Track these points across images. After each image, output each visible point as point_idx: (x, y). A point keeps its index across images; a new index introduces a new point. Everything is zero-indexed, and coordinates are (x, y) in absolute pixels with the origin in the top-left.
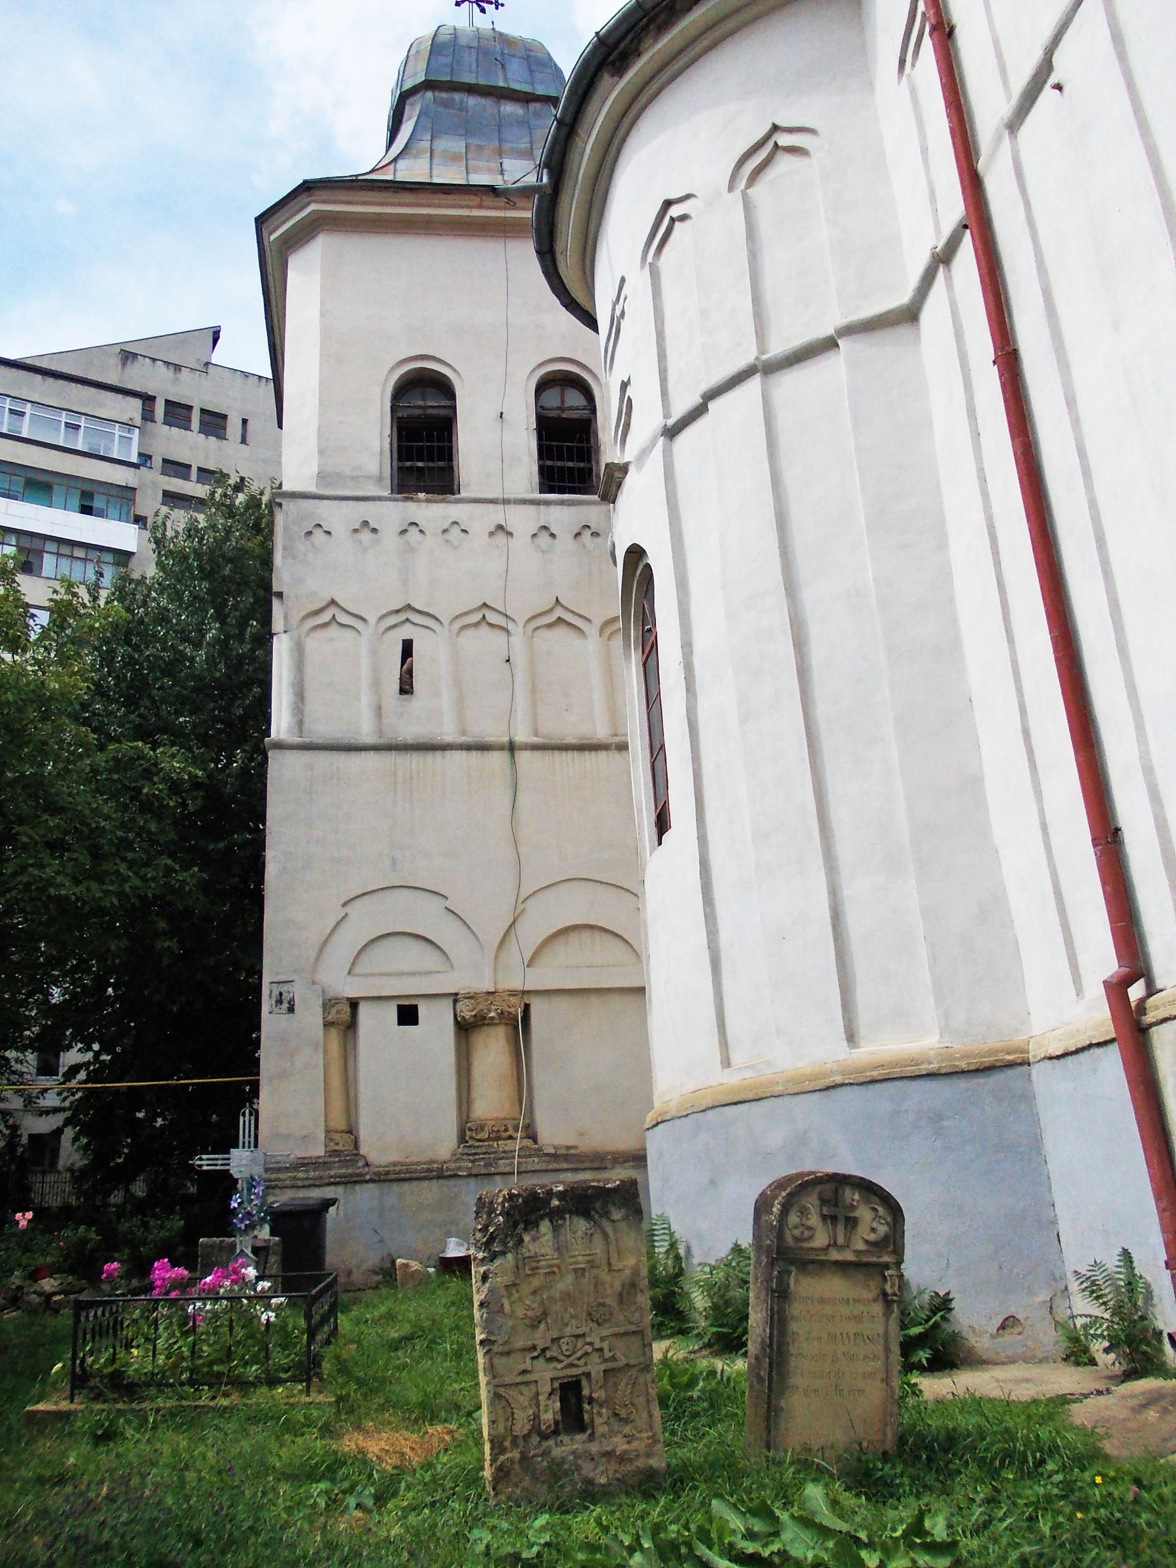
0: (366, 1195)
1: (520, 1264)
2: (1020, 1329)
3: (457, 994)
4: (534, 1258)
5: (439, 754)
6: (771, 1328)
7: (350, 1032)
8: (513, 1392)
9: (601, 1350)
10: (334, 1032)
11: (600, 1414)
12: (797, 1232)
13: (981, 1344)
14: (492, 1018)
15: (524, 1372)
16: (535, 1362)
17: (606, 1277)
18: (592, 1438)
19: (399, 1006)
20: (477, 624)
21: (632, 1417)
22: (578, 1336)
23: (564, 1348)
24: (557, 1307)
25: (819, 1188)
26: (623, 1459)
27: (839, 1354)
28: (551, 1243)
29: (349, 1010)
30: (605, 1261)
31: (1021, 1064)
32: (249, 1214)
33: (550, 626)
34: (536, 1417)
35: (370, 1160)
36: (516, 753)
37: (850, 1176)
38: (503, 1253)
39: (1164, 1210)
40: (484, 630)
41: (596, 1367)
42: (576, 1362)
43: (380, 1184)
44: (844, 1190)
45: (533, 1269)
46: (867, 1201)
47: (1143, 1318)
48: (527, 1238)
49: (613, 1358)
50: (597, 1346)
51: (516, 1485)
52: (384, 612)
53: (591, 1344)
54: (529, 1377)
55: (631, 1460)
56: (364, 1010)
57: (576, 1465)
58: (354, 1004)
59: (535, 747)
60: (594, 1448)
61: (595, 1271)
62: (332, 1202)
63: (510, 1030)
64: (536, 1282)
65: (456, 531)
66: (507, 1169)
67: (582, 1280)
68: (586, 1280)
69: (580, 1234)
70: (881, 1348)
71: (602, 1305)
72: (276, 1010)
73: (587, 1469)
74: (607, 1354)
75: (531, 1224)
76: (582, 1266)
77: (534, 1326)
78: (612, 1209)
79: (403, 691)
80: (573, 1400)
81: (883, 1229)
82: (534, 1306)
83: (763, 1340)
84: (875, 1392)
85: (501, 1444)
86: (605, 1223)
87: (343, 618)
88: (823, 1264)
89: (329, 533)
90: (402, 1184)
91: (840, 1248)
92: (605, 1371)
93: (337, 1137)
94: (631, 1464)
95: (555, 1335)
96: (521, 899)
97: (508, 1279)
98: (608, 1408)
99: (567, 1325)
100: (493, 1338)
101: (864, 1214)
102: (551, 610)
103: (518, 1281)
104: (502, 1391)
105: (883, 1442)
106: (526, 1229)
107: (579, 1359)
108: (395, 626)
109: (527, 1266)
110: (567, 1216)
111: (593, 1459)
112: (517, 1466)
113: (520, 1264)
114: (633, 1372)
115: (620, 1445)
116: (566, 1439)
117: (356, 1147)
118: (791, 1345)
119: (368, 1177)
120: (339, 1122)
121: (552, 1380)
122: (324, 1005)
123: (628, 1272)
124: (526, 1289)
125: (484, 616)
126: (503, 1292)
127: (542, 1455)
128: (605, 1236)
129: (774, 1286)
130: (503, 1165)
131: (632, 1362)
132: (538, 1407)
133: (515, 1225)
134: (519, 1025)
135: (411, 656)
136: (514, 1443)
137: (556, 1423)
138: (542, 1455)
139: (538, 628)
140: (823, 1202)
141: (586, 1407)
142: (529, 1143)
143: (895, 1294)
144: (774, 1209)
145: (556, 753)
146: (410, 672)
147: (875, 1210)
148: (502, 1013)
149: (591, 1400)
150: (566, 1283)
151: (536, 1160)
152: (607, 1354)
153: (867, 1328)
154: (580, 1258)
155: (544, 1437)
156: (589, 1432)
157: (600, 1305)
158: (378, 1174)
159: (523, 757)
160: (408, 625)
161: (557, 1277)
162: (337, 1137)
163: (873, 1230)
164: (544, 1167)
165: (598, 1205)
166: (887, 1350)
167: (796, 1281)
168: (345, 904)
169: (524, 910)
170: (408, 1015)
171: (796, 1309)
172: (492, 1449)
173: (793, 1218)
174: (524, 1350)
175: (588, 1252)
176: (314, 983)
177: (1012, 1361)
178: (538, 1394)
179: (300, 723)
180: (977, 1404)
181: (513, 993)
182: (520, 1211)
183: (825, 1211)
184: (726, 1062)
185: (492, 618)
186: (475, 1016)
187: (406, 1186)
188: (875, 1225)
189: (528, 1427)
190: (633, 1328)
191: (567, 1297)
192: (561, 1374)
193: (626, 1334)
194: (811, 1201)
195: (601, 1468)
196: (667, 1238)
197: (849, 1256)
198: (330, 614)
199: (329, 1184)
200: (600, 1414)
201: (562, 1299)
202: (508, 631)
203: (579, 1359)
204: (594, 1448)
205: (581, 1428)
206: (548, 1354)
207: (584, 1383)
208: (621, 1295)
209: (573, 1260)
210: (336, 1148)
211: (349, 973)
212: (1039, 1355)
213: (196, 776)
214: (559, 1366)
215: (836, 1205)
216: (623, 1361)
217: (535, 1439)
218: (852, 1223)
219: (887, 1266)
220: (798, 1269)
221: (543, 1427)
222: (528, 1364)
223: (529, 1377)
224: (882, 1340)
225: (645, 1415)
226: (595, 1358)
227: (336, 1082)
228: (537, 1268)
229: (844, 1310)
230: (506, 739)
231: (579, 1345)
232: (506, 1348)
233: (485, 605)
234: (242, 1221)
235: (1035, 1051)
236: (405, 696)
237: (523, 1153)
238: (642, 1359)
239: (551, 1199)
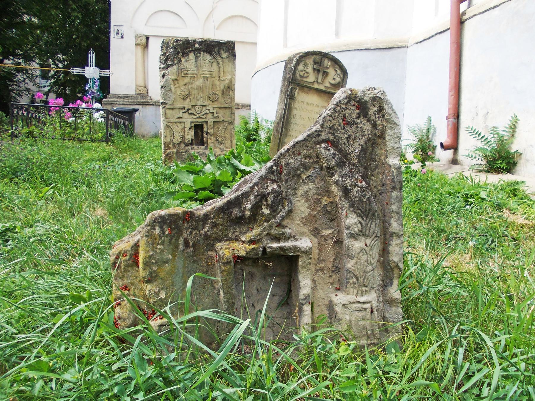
1: (180, 71)
8: (174, 125)
9: (213, 113)
10: (139, 47)
11: (210, 139)
12: (302, 74)
15: (179, 118)
16: (184, 114)
17: (217, 83)
18: (206, 148)
22: (203, 106)
23: (197, 110)
24: (195, 92)
25: (315, 56)
28: (194, 64)
29: (145, 40)
30: (217, 75)
31: (404, 47)
32: (93, 92)
34: (184, 137)
38: (172, 65)
39: (452, 96)
41: (210, 119)
45: (185, 74)
46: (334, 67)
47: (430, 141)
48: (183, 60)
49: (218, 117)
50: (211, 111)
53: (209, 110)
54: (181, 120)
56: (151, 40)
58: (147, 38)
61: (213, 79)
62: (137, 110)
64: (187, 80)
69: (207, 61)
72: (116, 37)
74: (215, 115)
75: (185, 55)
78: (222, 52)
80: (200, 133)
81: (338, 80)
82: (184, 90)
83: (281, 116)
85: (168, 146)
88: (310, 89)
93: (140, 88)
97: (174, 77)
98: (214, 137)
99: (199, 100)
104: (169, 124)
106: (183, 56)
107: (203, 115)
109: (182, 73)
110: (202, 52)
112: (174, 155)
113: (180, 71)
114: (226, 124)
116: (196, 147)
117: (147, 93)
118: (292, 119)
121: (191, 122)
122: (136, 37)
123: (227, 82)
124: (181, 83)
126: (171, 82)
128: (218, 63)
129: (288, 93)
131: (226, 120)
132: (185, 133)
133: (178, 53)
140: (315, 63)
141: (205, 135)
144: (293, 62)
149: (207, 133)
150: (199, 82)
152: (215, 115)
154: (207, 72)
155: (187, 145)
157: (214, 93)
158: (155, 102)
161: (196, 79)
162: (140, 88)
163: (334, 79)
165: (216, 50)
167: (298, 94)
171: (296, 105)
172: (165, 147)
173: (301, 67)
174: (180, 108)
176: (131, 27)
178: (185, 127)
182: (180, 48)
183: (315, 66)
184: (285, 46)
188: (335, 77)
189: (180, 140)
190: (227, 106)
191: (200, 88)
192: (194, 120)
193: (225, 108)
194: (310, 62)
197: (322, 87)
200: (210, 139)
201: (197, 89)
203: (203, 115)
205: (203, 144)
206: (190, 111)
207: (205, 126)
208: (223, 91)
209: (203, 72)
215: (320, 66)
216: (221, 119)
217: (183, 145)
218: (325, 74)
220: (300, 89)
221: (186, 141)
222: (181, 115)
223: (181, 120)
225: (229, 142)
226: (210, 116)
227: (140, 68)
228: (187, 74)
231: (204, 110)
232: (172, 107)
234: (90, 95)
235: (411, 41)
238: (230, 119)
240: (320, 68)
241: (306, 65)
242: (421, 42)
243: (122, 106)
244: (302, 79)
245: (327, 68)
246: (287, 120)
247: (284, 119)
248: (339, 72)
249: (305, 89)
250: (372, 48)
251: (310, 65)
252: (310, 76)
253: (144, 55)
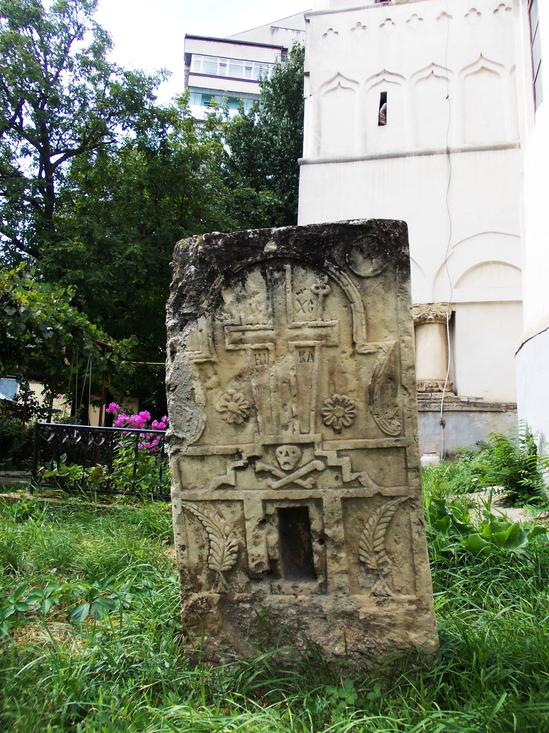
4: (239, 327)
5: (401, 159)
8: (210, 512)
9: (338, 468)
11: (335, 558)
14: (431, 319)
15: (224, 486)
16: (240, 474)
17: (349, 364)
18: (323, 589)
20: (428, 77)
21: (386, 570)
22: (303, 446)
23: (282, 459)
24: (271, 399)
26: (369, 625)
28: (263, 307)
30: (345, 338)
33: (476, 73)
34: (241, 550)
36: (451, 155)
38: (194, 317)
41: (330, 492)
42: (300, 481)
45: (235, 342)
48: (228, 298)
50: (333, 461)
51: (213, 634)
52: (369, 77)
53: (323, 458)
54: (229, 494)
55: (382, 630)
57: (299, 622)
59: (464, 151)
60: (327, 603)
61: (332, 352)
63: (442, 328)
64: (242, 362)
65: (415, 19)
66: (436, 409)
67: (310, 364)
68: (316, 364)
71: (343, 403)
73: (316, 631)
75: (235, 278)
76: (311, 343)
77: (237, 426)
79: (380, 124)
85: (194, 579)
86: (346, 280)
87: (344, 84)
89: (336, 33)
92: (344, 500)
94: (382, 635)
95: (269, 440)
99: (286, 427)
100: (181, 435)
102: (477, 62)
103: (214, 358)
104: (193, 507)
106: (227, 284)
107: (304, 477)
108: (376, 85)
110: (288, 267)
111: (325, 618)
113: (218, 333)
114: (391, 506)
115: (368, 607)
116: (287, 585)
121: (265, 502)
123: (382, 357)
124: (226, 371)
125: (433, 71)
126: (193, 371)
127: (251, 601)
130: (433, 407)
131: (388, 491)
132: (245, 536)
134: (449, 324)
136: (212, 575)
137: (272, 562)
138: (251, 601)
139: (468, 75)
141: (316, 546)
142: (451, 394)
145: (478, 153)
146: (385, 112)
148: (437, 316)
149: (323, 539)
150: (284, 366)
151: (455, 404)
152: (348, 476)
154: (308, 331)
156: (320, 580)
157: (337, 402)
160: (384, 83)
161: (272, 357)
164: (459, 408)
165: (336, 253)
169: (453, 253)
174: (224, 456)
175: (319, 322)
178: (243, 520)
179: (319, 148)
181: (444, 304)
182: (219, 258)
185: (437, 72)
186: (420, 318)
189: (230, 561)
190: (387, 442)
191: (288, 388)
192: (276, 495)
193: (380, 450)
195: (338, 632)
196: (525, 428)
198: (338, 81)
200: (335, 558)
201: (277, 389)
202: (447, 79)
203: (304, 477)
204: (327, 603)
207: (313, 512)
208: (370, 392)
213: (279, 204)
214: (276, 484)
217: (241, 579)
221: (252, 565)
222: (229, 477)
223: (229, 494)
225: (406, 569)
226: (329, 478)
228: (241, 341)
230: (444, 148)
232: (198, 450)
233: (433, 64)
236: (381, 127)
237: (447, 400)
239: (266, 241)
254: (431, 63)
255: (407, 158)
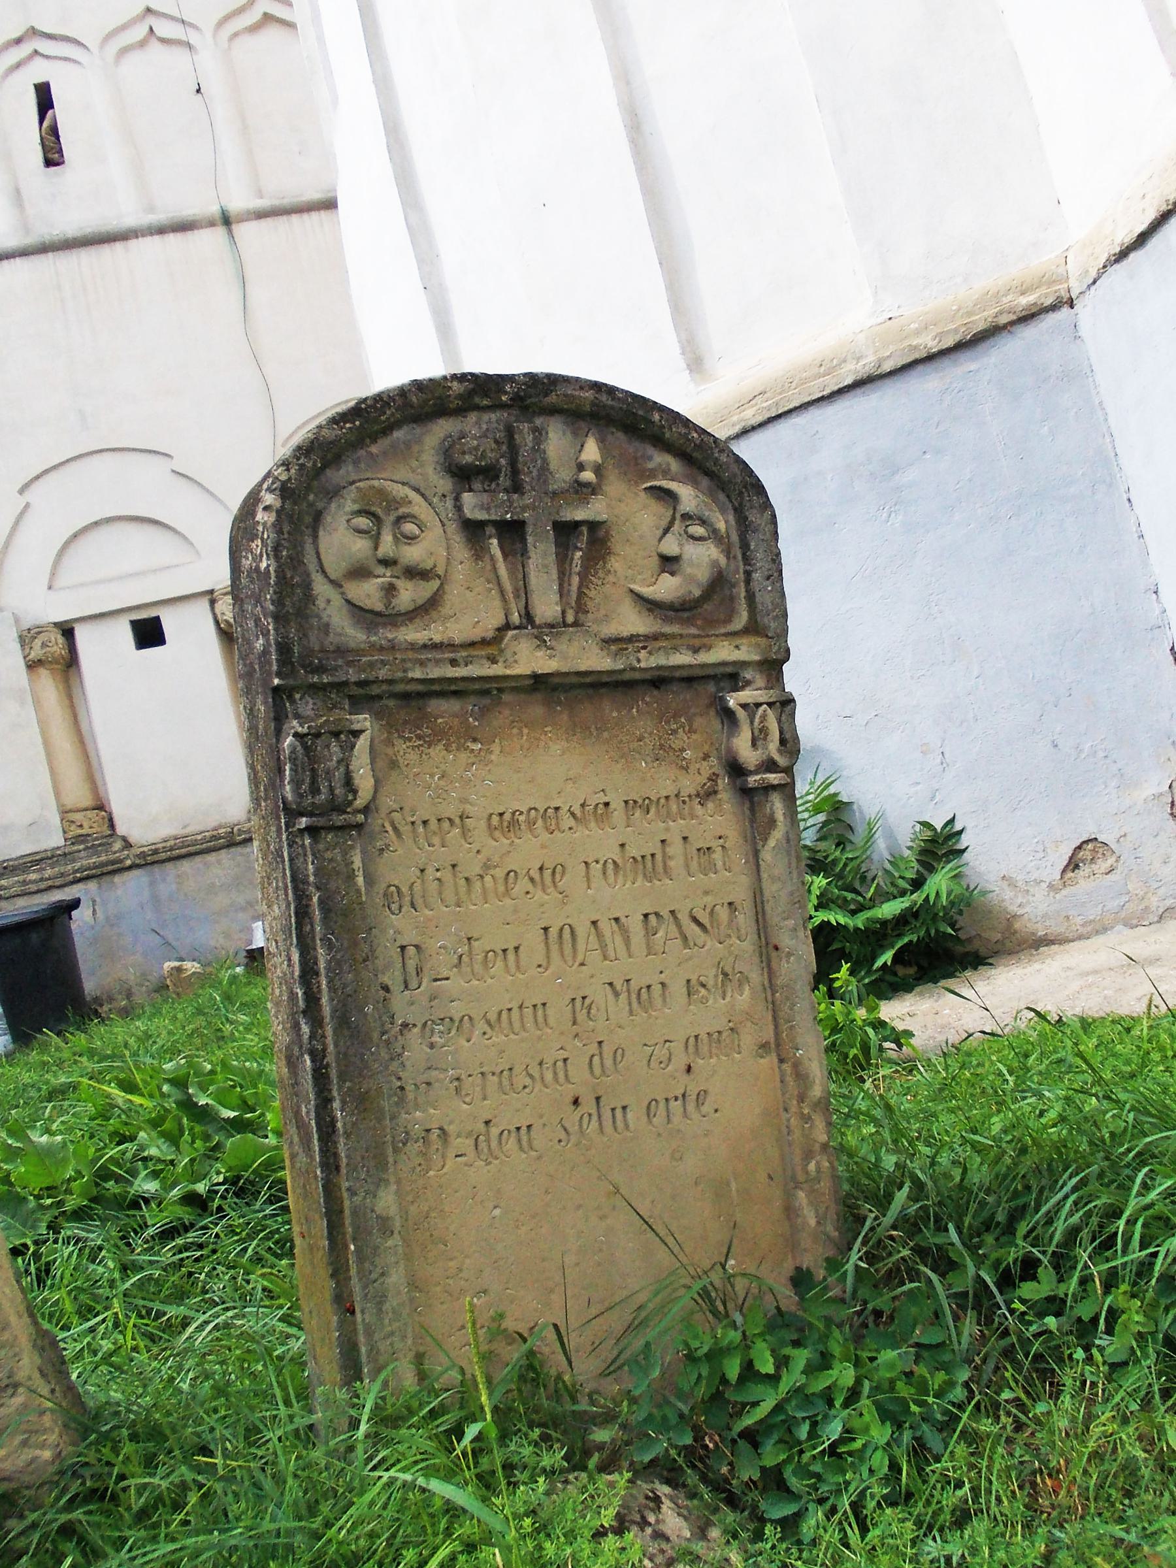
0: (130, 889)
2: (1111, 861)
3: (212, 592)
5: (119, 246)
6: (306, 948)
7: (73, 669)
10: (43, 672)
12: (368, 592)
13: (1034, 908)
19: (133, 623)
20: (142, 44)
25: (443, 427)
27: (599, 994)
29: (61, 640)
31: (1054, 308)
33: (254, 28)
35: (131, 840)
36: (234, 227)
37: (553, 381)
40: (155, 47)
43: (149, 868)
44: (539, 434)
46: (637, 471)
56: (82, 635)
58: (67, 631)
59: (261, 215)
62: (75, 904)
70: (747, 946)
79: (49, 163)
81: (702, 557)
84: (739, 1091)
88: (488, 691)
90: (178, 863)
91: (544, 633)
93: (78, 817)
96: (279, 441)
101: (627, 510)
105: (792, 1244)
108: (18, 66)
117: (112, 825)
119: (128, 862)
120: (78, 795)
122: (22, 639)
135: (52, 107)
143: (770, 766)
145: (295, 218)
146: (54, 131)
147: (667, 496)
153: (681, 891)
158: (143, 855)
159: (244, 231)
160: (38, 61)
162: (78, 817)
163: (669, 563)
166: (768, 949)
168: (21, 491)
170: (149, 633)
173: (340, 540)
177: (1100, 929)
180: (1055, 1039)
185: (165, 29)
187: (186, 866)
188: (670, 546)
194: (414, 474)
197: (584, 656)
199: (80, 880)
202: (189, 46)
210: (80, 831)
211: (50, 588)
212: (1155, 903)
218: (582, 542)
219: (732, 677)
224: (744, 920)
229: (601, 842)
230: (214, 209)
233: (149, 10)
240: (524, 507)
241: (378, 513)
242: (1142, 239)
243: (21, 902)
244: (387, 634)
245: (583, 491)
246: (343, 1021)
247: (317, 1022)
248: (688, 496)
249: (444, 709)
250: (887, 367)
251: (419, 506)
252: (455, 595)
253: (70, 697)
254: (140, 9)
255: (133, 243)
